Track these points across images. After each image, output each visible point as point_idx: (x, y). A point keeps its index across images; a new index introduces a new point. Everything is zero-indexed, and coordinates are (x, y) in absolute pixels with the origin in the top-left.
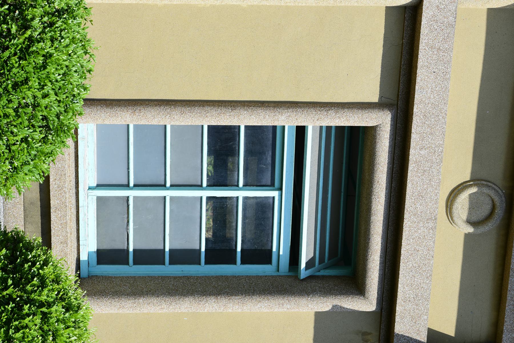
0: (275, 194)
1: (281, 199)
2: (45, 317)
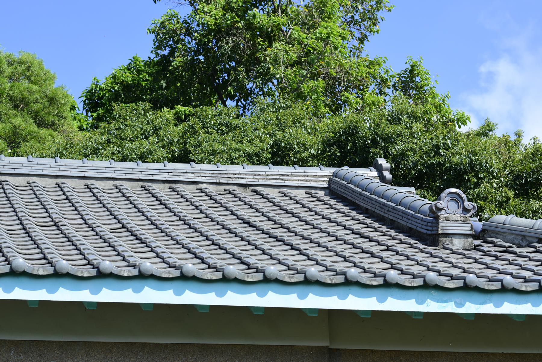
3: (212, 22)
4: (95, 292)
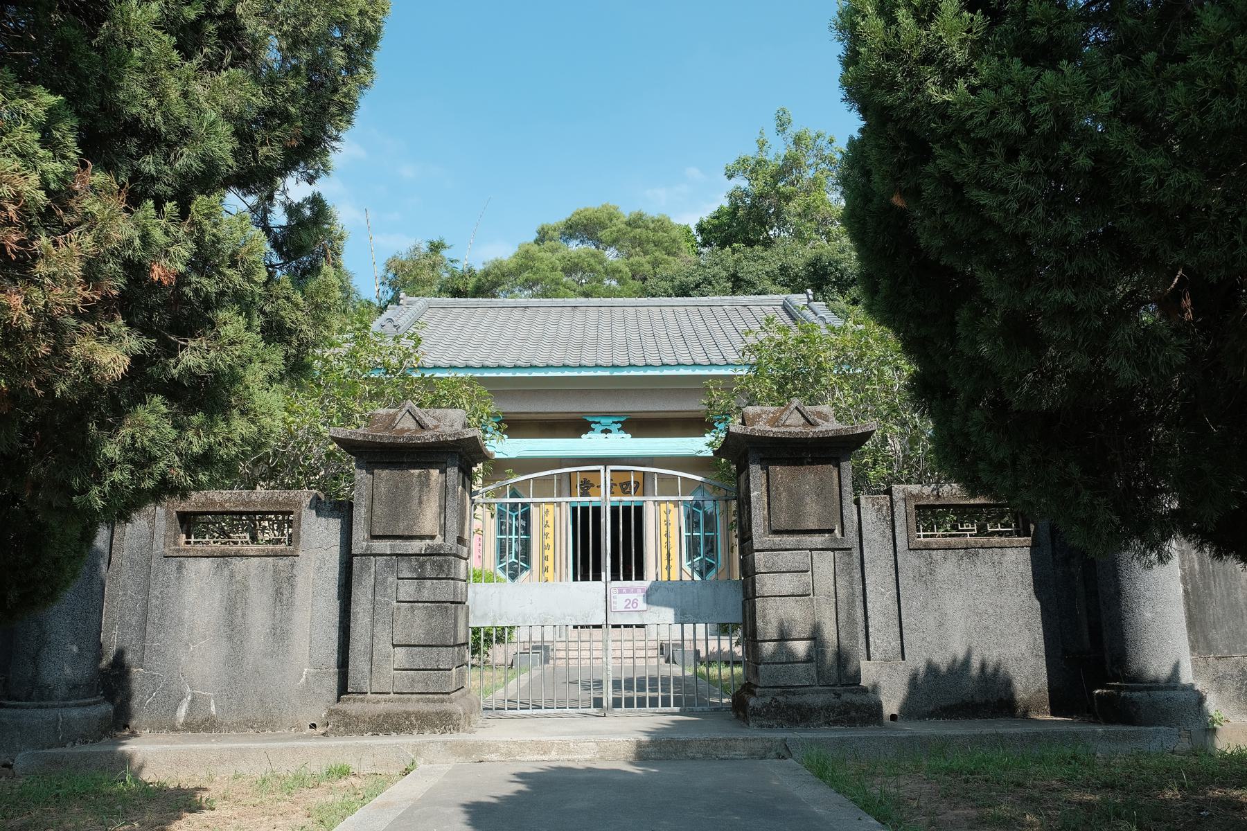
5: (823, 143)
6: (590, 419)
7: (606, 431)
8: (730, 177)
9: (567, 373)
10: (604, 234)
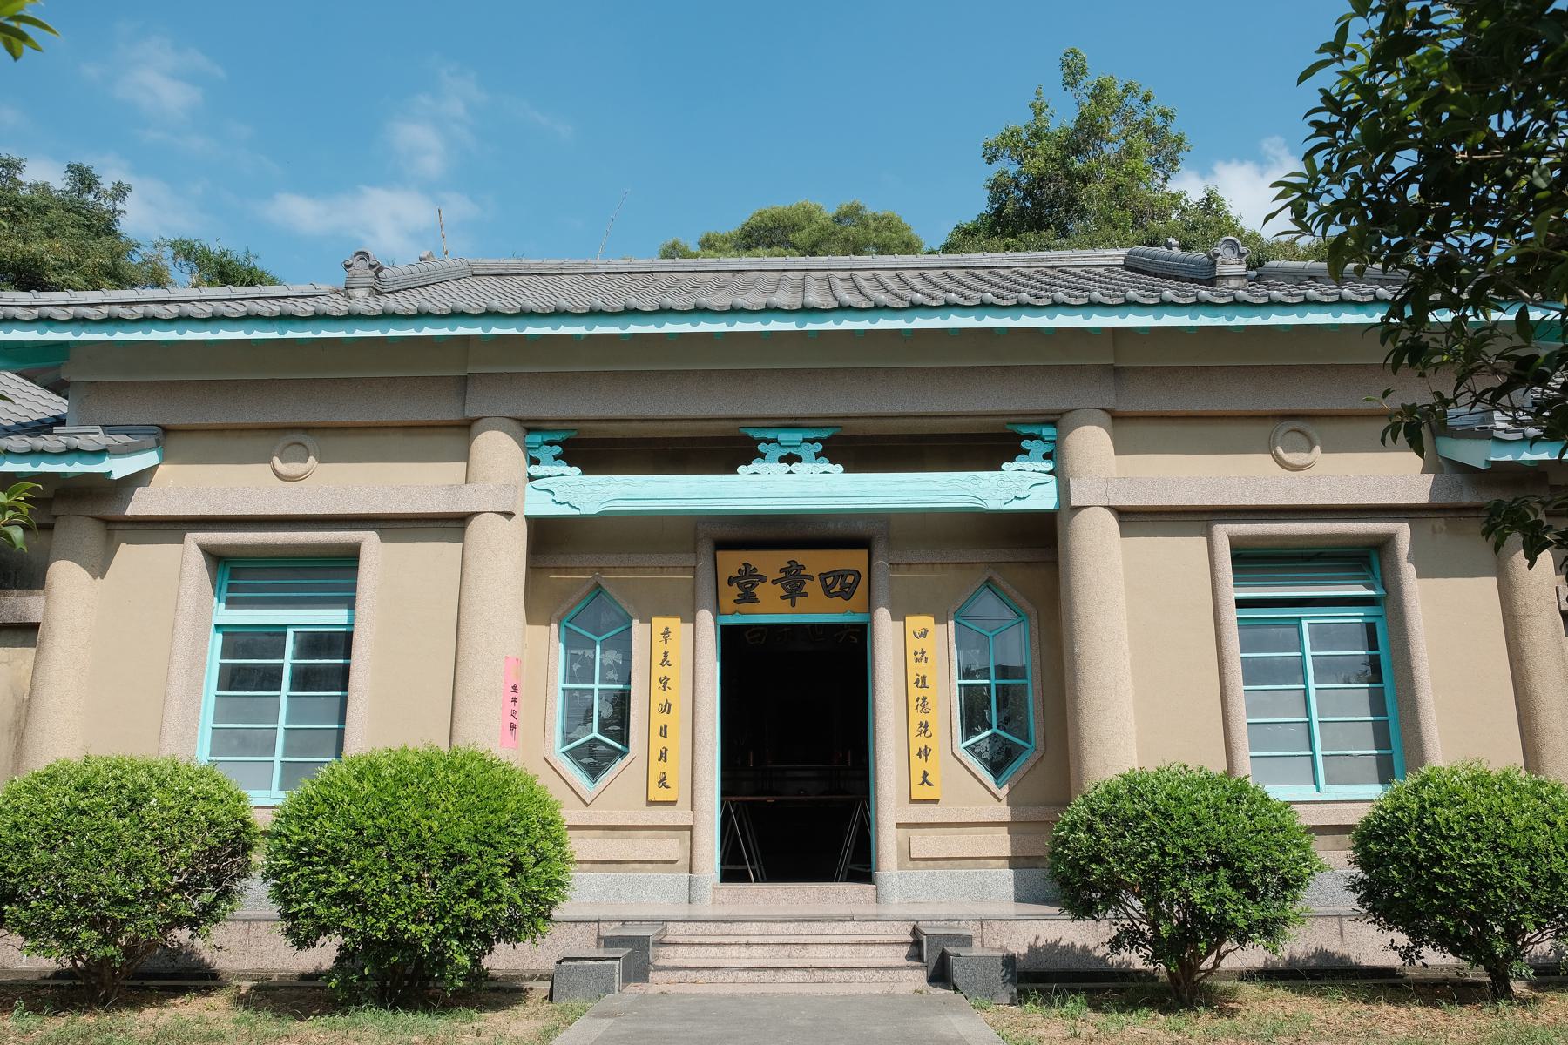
0: (1305, 623)
1: (1309, 618)
2: (1434, 804)
3: (1035, 172)
4: (909, 321)
5: (1134, 102)
6: (756, 435)
7: (790, 459)
8: (990, 161)
9: (705, 327)
10: (797, 237)
